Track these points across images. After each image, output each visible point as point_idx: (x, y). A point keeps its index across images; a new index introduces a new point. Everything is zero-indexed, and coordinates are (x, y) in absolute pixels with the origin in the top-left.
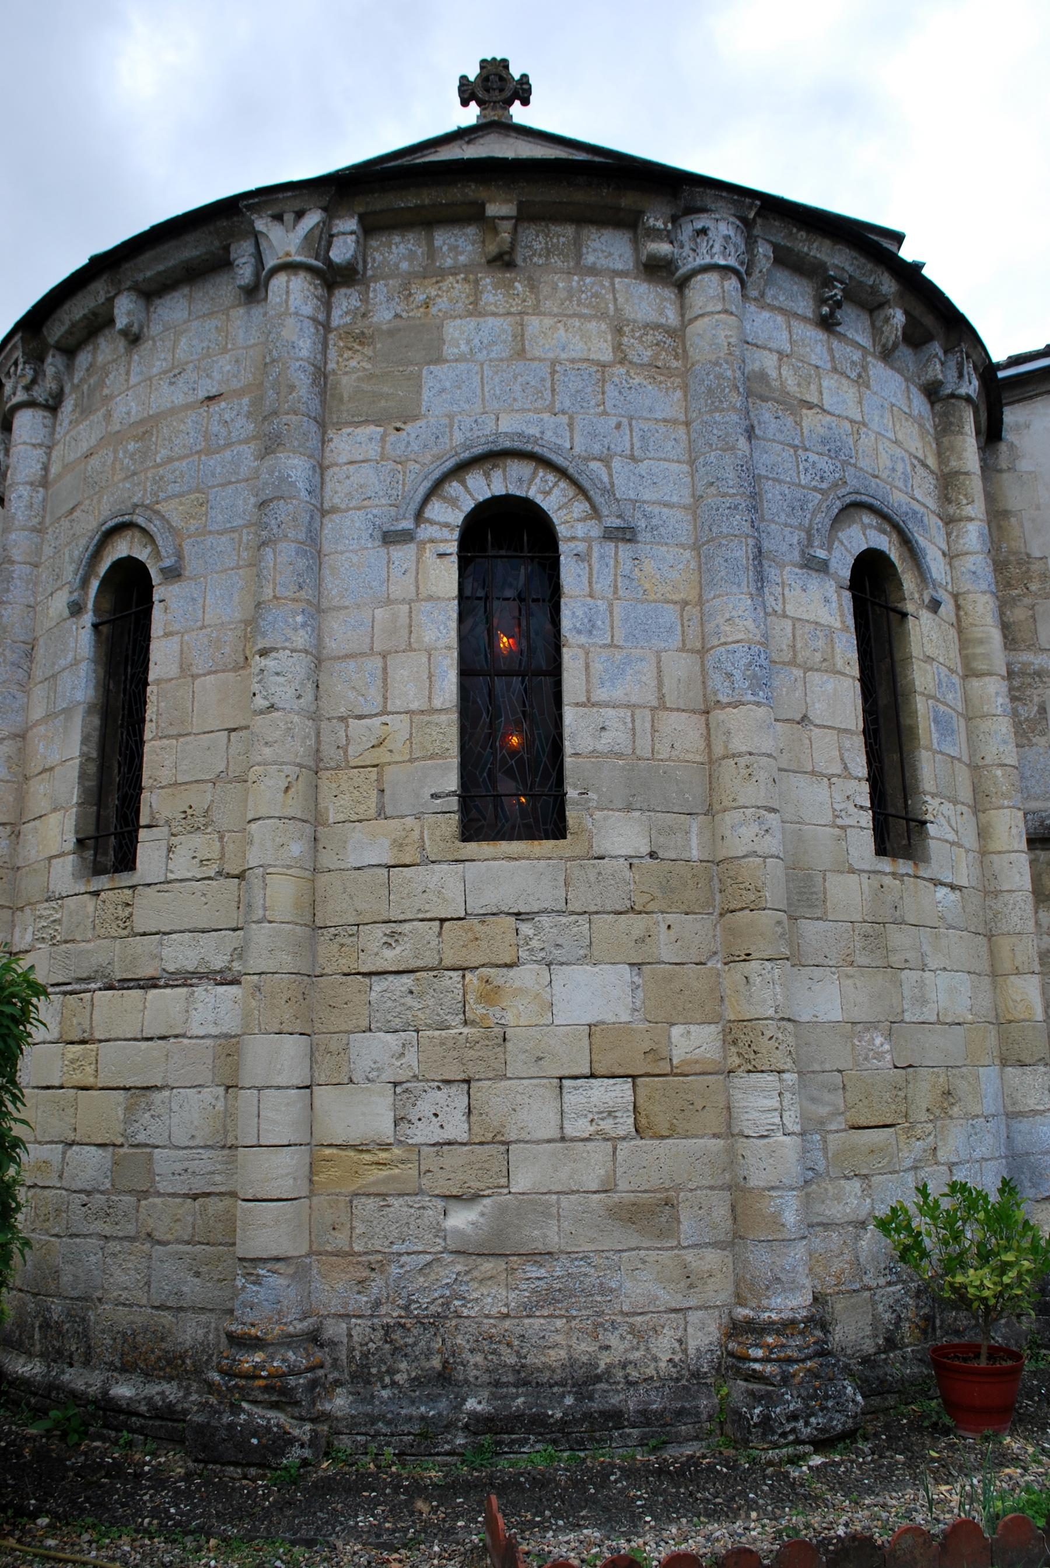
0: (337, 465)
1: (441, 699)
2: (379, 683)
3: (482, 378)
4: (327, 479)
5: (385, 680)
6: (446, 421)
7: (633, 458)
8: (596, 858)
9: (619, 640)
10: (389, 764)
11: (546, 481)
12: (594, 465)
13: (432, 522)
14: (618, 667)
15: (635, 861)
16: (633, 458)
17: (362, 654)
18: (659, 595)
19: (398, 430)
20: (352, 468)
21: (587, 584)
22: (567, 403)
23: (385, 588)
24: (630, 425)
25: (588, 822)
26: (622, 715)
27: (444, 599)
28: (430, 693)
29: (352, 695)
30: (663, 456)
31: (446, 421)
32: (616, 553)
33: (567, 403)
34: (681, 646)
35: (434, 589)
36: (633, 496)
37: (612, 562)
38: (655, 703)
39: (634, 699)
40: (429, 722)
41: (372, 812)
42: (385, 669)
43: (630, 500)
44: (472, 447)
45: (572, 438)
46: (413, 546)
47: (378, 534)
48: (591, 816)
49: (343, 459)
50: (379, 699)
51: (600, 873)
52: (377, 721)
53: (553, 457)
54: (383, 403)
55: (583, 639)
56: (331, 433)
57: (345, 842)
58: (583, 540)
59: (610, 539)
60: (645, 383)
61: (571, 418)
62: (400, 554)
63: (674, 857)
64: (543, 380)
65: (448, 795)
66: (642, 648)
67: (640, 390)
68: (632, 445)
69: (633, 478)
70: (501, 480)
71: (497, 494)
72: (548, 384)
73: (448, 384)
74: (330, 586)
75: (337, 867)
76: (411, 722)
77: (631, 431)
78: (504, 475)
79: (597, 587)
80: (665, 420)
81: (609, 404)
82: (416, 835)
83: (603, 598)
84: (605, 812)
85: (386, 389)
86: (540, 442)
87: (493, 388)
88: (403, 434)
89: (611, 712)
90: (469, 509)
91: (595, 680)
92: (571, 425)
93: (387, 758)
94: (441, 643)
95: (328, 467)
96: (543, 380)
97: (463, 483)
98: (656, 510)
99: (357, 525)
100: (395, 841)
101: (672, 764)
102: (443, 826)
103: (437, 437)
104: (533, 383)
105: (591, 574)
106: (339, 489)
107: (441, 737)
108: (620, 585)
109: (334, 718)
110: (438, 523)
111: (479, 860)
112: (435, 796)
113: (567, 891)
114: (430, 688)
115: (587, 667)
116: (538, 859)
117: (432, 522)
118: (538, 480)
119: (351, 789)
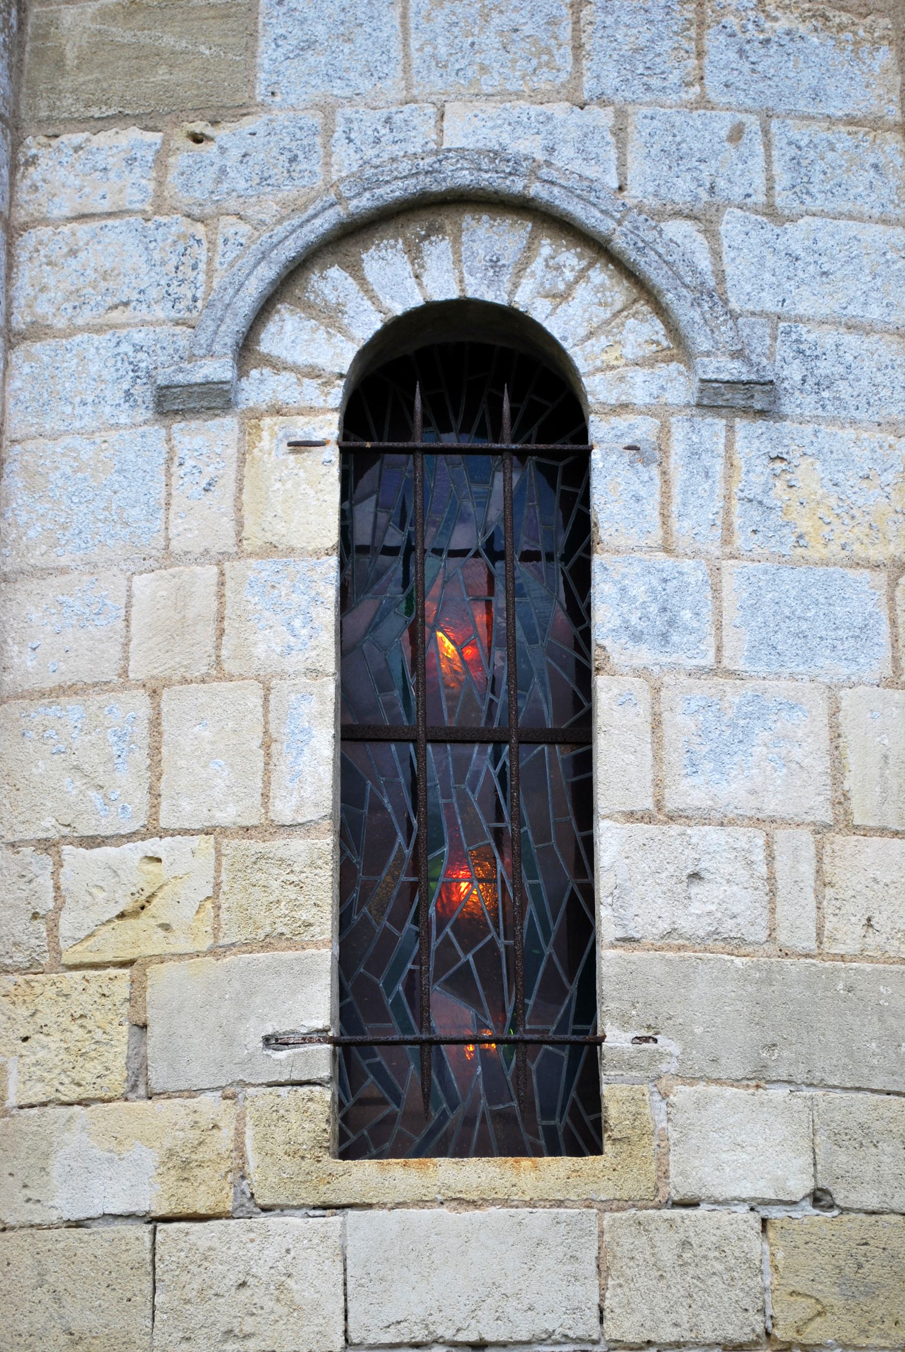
0: (45, 221)
1: (294, 800)
2: (141, 757)
3: (404, 16)
4: (23, 256)
5: (155, 750)
6: (315, 119)
7: (771, 212)
8: (677, 1204)
9: (735, 659)
10: (162, 959)
11: (558, 268)
12: (676, 229)
13: (276, 365)
14: (733, 725)
15: (775, 1213)
16: (771, 212)
17: (101, 686)
18: (834, 547)
19: (197, 139)
20: (83, 230)
21: (658, 520)
22: (611, 80)
23: (159, 524)
24: (766, 132)
25: (656, 1112)
26: (743, 843)
27: (304, 553)
28: (267, 783)
29: (72, 786)
30: (846, 207)
31: (315, 119)
32: (730, 444)
33: (611, 80)
34: (889, 672)
35: (280, 528)
36: (770, 304)
37: (718, 467)
38: (825, 815)
39: (772, 806)
40: (261, 857)
41: (117, 1080)
42: (155, 724)
43: (763, 314)
44: (379, 184)
45: (622, 164)
46: (229, 423)
47: (144, 392)
48: (665, 1096)
49: (62, 207)
50: (141, 798)
51: (686, 1244)
52: (134, 851)
53: (577, 210)
54: (162, 74)
55: (644, 655)
56: (32, 145)
57: (47, 1156)
58: (649, 411)
59: (714, 409)
60: (803, 29)
61: (621, 114)
62: (198, 441)
63: (874, 1204)
64: (552, 22)
65: (306, 1039)
66: (792, 676)
67: (791, 47)
68: (770, 179)
69: (771, 261)
70: (447, 264)
71: (439, 296)
72: (566, 33)
73: (320, 30)
74: (23, 518)
75: (24, 1218)
76: (219, 854)
77: (768, 146)
78: (456, 252)
79: (681, 527)
80: (851, 121)
81: (714, 81)
82: (224, 1139)
83: (696, 554)
84: (701, 1087)
85: (168, 40)
86: (544, 172)
87: (432, 41)
88: (209, 150)
89: (713, 835)
90: (369, 334)
91: (675, 757)
92: (619, 132)
93: (155, 944)
94: (296, 662)
95: (25, 227)
96: (552, 22)
97: (355, 270)
98: (828, 338)
99: (94, 369)
100: (171, 1153)
101: (868, 967)
102: (293, 1117)
103: (294, 159)
104: (527, 30)
105: (666, 495)
106: (51, 282)
107: (291, 893)
108: (737, 522)
109: (25, 842)
110: (293, 368)
111: (382, 1206)
112: (273, 1041)
113: (603, 1288)
114: (267, 771)
115: (657, 723)
116: (531, 1204)
117: (276, 365)
118: (537, 265)
119: (66, 1020)
